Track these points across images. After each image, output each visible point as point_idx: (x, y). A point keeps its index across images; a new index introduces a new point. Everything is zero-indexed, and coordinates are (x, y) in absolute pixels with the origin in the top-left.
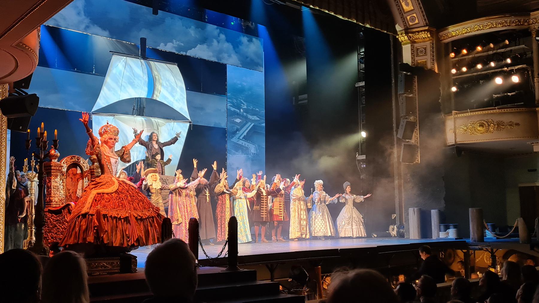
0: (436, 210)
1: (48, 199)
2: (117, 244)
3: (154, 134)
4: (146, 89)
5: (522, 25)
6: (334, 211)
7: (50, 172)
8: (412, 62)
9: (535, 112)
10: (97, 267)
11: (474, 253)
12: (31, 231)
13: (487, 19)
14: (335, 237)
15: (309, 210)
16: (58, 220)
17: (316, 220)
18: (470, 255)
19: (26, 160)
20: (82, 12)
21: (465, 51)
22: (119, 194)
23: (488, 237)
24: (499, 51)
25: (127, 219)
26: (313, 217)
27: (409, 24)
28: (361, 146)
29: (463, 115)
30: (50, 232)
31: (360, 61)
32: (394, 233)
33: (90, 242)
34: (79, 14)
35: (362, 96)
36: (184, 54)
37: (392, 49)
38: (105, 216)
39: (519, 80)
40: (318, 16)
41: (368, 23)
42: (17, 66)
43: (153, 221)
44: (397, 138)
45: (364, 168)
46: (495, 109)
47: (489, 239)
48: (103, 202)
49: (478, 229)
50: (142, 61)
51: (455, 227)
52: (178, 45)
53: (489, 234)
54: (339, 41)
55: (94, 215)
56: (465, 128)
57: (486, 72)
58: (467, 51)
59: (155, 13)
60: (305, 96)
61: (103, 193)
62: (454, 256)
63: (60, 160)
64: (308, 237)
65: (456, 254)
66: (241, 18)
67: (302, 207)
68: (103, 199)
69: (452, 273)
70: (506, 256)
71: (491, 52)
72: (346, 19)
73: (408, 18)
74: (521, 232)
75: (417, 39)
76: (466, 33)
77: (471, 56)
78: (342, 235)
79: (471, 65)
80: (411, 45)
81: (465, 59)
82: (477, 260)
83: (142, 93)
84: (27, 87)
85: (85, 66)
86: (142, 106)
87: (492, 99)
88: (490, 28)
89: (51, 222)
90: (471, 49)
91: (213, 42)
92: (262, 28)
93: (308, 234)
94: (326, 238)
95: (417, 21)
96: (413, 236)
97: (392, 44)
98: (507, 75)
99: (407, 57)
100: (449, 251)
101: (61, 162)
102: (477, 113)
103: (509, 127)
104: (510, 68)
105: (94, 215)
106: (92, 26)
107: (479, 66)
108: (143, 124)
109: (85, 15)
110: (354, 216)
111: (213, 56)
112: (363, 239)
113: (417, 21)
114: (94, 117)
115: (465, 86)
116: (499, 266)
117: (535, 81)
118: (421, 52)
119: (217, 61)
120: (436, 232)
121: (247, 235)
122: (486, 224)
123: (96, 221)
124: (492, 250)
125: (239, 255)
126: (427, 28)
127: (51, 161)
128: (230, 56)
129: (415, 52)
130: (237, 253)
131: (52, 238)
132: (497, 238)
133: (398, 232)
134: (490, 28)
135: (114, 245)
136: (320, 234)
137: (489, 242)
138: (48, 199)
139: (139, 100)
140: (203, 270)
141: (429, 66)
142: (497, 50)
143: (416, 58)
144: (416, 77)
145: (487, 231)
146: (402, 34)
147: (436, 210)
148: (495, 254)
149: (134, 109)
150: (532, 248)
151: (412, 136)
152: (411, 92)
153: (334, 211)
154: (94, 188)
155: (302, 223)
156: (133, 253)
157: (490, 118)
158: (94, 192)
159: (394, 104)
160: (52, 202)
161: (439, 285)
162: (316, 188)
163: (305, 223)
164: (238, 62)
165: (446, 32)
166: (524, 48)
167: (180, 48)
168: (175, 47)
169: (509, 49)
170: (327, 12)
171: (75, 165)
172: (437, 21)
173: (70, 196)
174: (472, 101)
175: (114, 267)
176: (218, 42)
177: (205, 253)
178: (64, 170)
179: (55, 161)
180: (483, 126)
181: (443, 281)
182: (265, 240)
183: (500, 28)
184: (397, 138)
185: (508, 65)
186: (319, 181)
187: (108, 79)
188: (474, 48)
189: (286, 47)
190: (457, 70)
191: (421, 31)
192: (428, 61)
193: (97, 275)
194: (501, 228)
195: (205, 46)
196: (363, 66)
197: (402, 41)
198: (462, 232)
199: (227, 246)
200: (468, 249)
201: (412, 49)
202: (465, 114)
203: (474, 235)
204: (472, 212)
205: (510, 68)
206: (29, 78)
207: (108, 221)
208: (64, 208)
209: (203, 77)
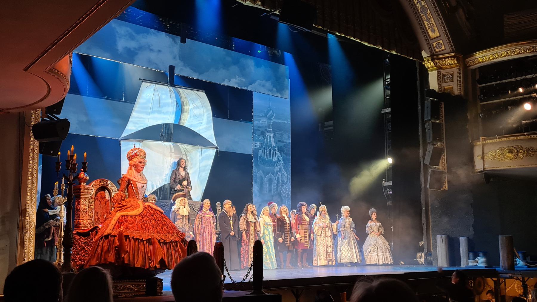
0: (465, 238)
1: (77, 222)
2: (138, 265)
3: (182, 160)
4: (174, 116)
6: (361, 235)
7: (80, 195)
8: (439, 88)
10: (123, 289)
11: (505, 281)
12: (60, 254)
13: (514, 45)
14: (361, 264)
15: (335, 237)
16: (86, 242)
17: (342, 247)
19: (56, 184)
20: (178, 57)
22: (143, 217)
23: (518, 265)
25: (149, 241)
26: (339, 243)
27: (435, 50)
29: (491, 141)
30: (78, 254)
31: (386, 88)
32: (422, 260)
33: (110, 263)
34: (175, 58)
35: (388, 122)
36: (245, 88)
37: (418, 75)
38: (127, 237)
40: (344, 43)
41: (394, 50)
42: (49, 92)
43: (177, 246)
44: (424, 164)
45: (390, 194)
48: (126, 224)
49: (508, 257)
50: (171, 88)
51: (484, 255)
52: (240, 80)
53: (520, 263)
55: (116, 236)
56: (494, 154)
57: (515, 98)
60: (331, 123)
61: (127, 216)
62: (484, 284)
63: (88, 183)
64: (334, 263)
65: (485, 283)
66: (267, 46)
67: (327, 234)
68: (127, 221)
72: (372, 46)
73: (434, 44)
75: (443, 65)
76: (493, 59)
78: (368, 262)
80: (438, 72)
82: (508, 289)
83: (170, 119)
85: (115, 93)
86: (169, 132)
87: (521, 125)
88: (517, 54)
92: (288, 56)
93: (334, 261)
94: (352, 264)
95: (443, 48)
96: (441, 262)
97: (418, 70)
99: (433, 84)
100: (479, 279)
101: (90, 186)
102: (505, 139)
105: (116, 236)
108: (171, 148)
109: (180, 59)
110: (379, 243)
112: (390, 267)
113: (443, 48)
114: (123, 143)
115: (493, 112)
116: (530, 296)
118: (448, 78)
120: (465, 259)
121: (272, 262)
122: (516, 252)
123: (119, 243)
124: (523, 278)
125: (264, 279)
127: (80, 184)
129: (441, 79)
130: (262, 277)
131: (80, 260)
132: (529, 267)
133: (426, 259)
134: (517, 54)
135: (136, 266)
136: (346, 261)
137: (520, 271)
138: (77, 222)
139: (166, 126)
140: (227, 293)
143: (443, 85)
145: (517, 259)
146: (428, 60)
147: (465, 238)
148: (527, 283)
149: (162, 135)
151: (439, 162)
153: (361, 235)
154: (119, 210)
155: (328, 250)
156: (158, 276)
157: (519, 145)
158: (119, 214)
159: (420, 130)
160: (80, 224)
162: (342, 215)
163: (331, 249)
165: (473, 58)
170: (352, 38)
171: (104, 188)
172: (463, 49)
173: (98, 218)
174: (501, 127)
175: (140, 289)
177: (230, 277)
178: (93, 193)
179: (83, 184)
180: (512, 153)
182: (290, 266)
183: (528, 54)
184: (424, 164)
186: (345, 207)
187: (137, 106)
189: (312, 75)
191: (448, 57)
193: (124, 297)
196: (389, 92)
197: (429, 68)
198: (492, 260)
199: (252, 272)
200: (499, 278)
201: (438, 76)
202: (493, 140)
203: (504, 263)
204: (501, 240)
207: (130, 241)
208: (92, 230)
209: (230, 105)
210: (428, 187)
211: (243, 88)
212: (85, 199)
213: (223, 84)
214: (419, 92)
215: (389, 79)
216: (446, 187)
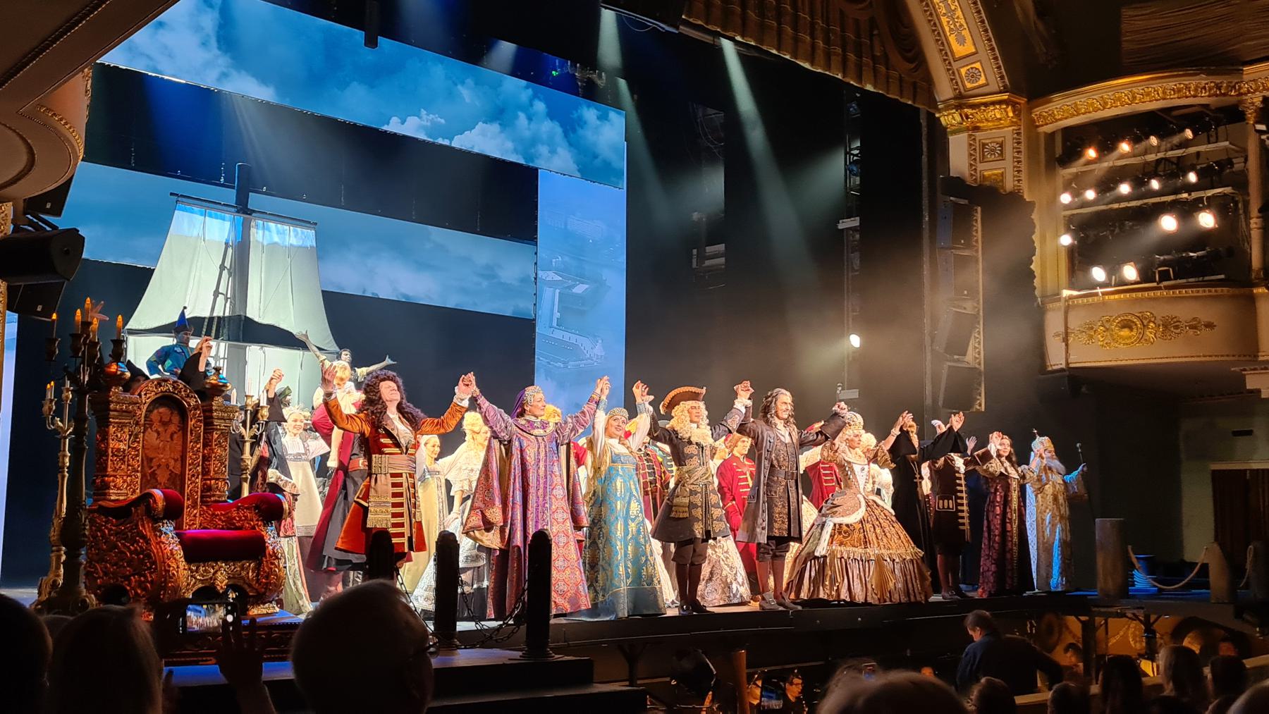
5: (1224, 95)
9: (1252, 299)
11: (1106, 623)
18: (1095, 629)
20: (213, 42)
21: (1091, 153)
23: (1138, 586)
24: (1170, 154)
27: (964, 86)
30: (103, 560)
36: (446, 142)
39: (1216, 222)
46: (1160, 288)
52: (432, 121)
53: (1141, 580)
54: (805, 119)
58: (1097, 151)
59: (371, 42)
60: (721, 247)
65: (1064, 626)
69: (1055, 673)
70: (1178, 633)
71: (1151, 157)
73: (963, 71)
74: (1217, 579)
77: (1106, 165)
79: (1106, 184)
80: (970, 136)
82: (1113, 641)
84: (58, 213)
89: (103, 535)
90: (1107, 147)
91: (517, 117)
95: (982, 81)
97: (924, 130)
98: (1186, 211)
99: (959, 159)
103: (1191, 332)
104: (1195, 195)
106: (234, 72)
107: (1125, 189)
109: (219, 48)
111: (516, 151)
117: (1253, 226)
118: (993, 151)
119: (522, 162)
124: (1147, 617)
126: (1005, 96)
128: (553, 152)
129: (979, 152)
141: (1009, 185)
142: (1166, 151)
143: (980, 167)
144: (979, 209)
145: (1135, 572)
150: (1238, 615)
152: (968, 246)
161: (1020, 700)
164: (572, 167)
166: (1226, 149)
167: (434, 129)
168: (425, 128)
169: (1192, 150)
172: (1032, 78)
173: (153, 474)
176: (530, 119)
180: (1131, 329)
181: (1033, 689)
185: (1190, 188)
191: (993, 103)
192: (1004, 171)
194: (1170, 568)
195: (495, 127)
196: (506, 49)
205: (1195, 195)
206: (64, 189)
208: (135, 503)
212: (121, 426)
214: (925, 182)
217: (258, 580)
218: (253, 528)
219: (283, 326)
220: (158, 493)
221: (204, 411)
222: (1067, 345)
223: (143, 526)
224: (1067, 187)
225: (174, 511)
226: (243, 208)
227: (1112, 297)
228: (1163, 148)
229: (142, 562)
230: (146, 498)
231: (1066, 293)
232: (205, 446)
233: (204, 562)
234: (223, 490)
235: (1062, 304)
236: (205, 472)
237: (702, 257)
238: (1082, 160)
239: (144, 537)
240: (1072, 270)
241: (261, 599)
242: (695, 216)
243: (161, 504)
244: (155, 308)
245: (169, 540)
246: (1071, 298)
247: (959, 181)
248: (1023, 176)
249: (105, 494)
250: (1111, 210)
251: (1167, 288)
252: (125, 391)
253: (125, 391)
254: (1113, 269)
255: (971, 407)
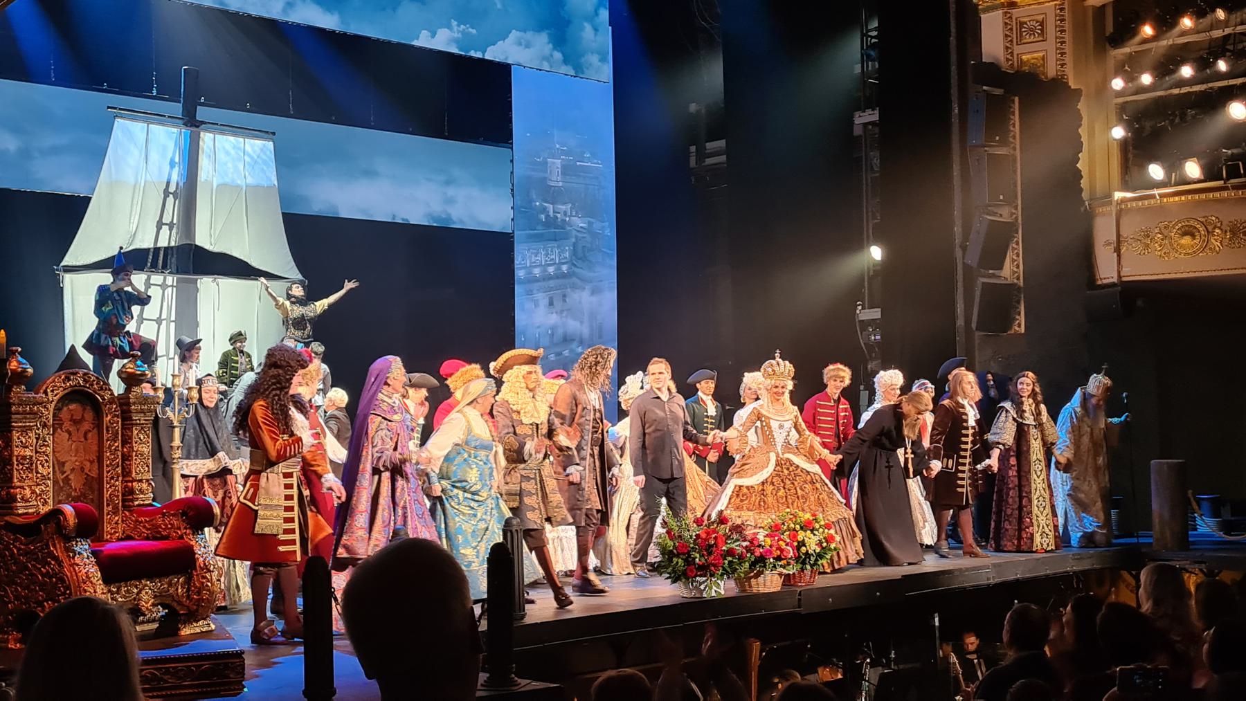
8: (1008, 60)
21: (1148, 30)
28: (870, 284)
30: (12, 583)
31: (865, 57)
36: (479, 55)
47: (1202, 535)
52: (463, 32)
53: (1205, 526)
58: (1154, 28)
60: (722, 143)
71: (1218, 33)
79: (1165, 67)
81: (1150, 50)
107: (1187, 71)
118: (1032, 31)
129: (1016, 32)
143: (1017, 49)
144: (1017, 99)
152: (1004, 142)
160: (15, 500)
173: (67, 480)
178: (48, 413)
180: (1193, 236)
188: (1174, 23)
190: (1126, 82)
196: (872, 66)
210: (974, 325)
211: (473, 54)
212: (25, 430)
213: (415, 43)
214: (953, 68)
215: (875, 29)
216: (1019, 325)
217: (188, 597)
218: (181, 537)
219: (234, 254)
220: (68, 509)
221: (121, 405)
222: (1119, 256)
223: (54, 546)
224: (1119, 71)
225: (89, 527)
226: (191, 121)
227: (1171, 199)
228: (1232, 22)
229: (55, 585)
230: (56, 513)
231: (1118, 195)
232: (124, 443)
233: (126, 581)
234: (145, 497)
235: (1114, 209)
236: (126, 473)
237: (702, 155)
238: (1137, 39)
239: (56, 559)
240: (1126, 168)
241: (193, 617)
242: (693, 107)
243: (72, 521)
244: (94, 240)
245: (84, 562)
246: (1123, 201)
247: (993, 67)
248: (1068, 59)
249: (12, 508)
250: (1171, 95)
251: (1236, 187)
252: (28, 390)
253: (28, 390)
254: (1173, 166)
255: (1010, 328)
